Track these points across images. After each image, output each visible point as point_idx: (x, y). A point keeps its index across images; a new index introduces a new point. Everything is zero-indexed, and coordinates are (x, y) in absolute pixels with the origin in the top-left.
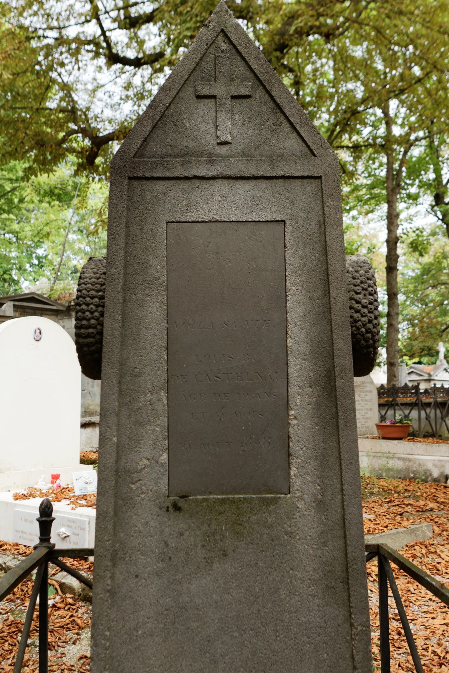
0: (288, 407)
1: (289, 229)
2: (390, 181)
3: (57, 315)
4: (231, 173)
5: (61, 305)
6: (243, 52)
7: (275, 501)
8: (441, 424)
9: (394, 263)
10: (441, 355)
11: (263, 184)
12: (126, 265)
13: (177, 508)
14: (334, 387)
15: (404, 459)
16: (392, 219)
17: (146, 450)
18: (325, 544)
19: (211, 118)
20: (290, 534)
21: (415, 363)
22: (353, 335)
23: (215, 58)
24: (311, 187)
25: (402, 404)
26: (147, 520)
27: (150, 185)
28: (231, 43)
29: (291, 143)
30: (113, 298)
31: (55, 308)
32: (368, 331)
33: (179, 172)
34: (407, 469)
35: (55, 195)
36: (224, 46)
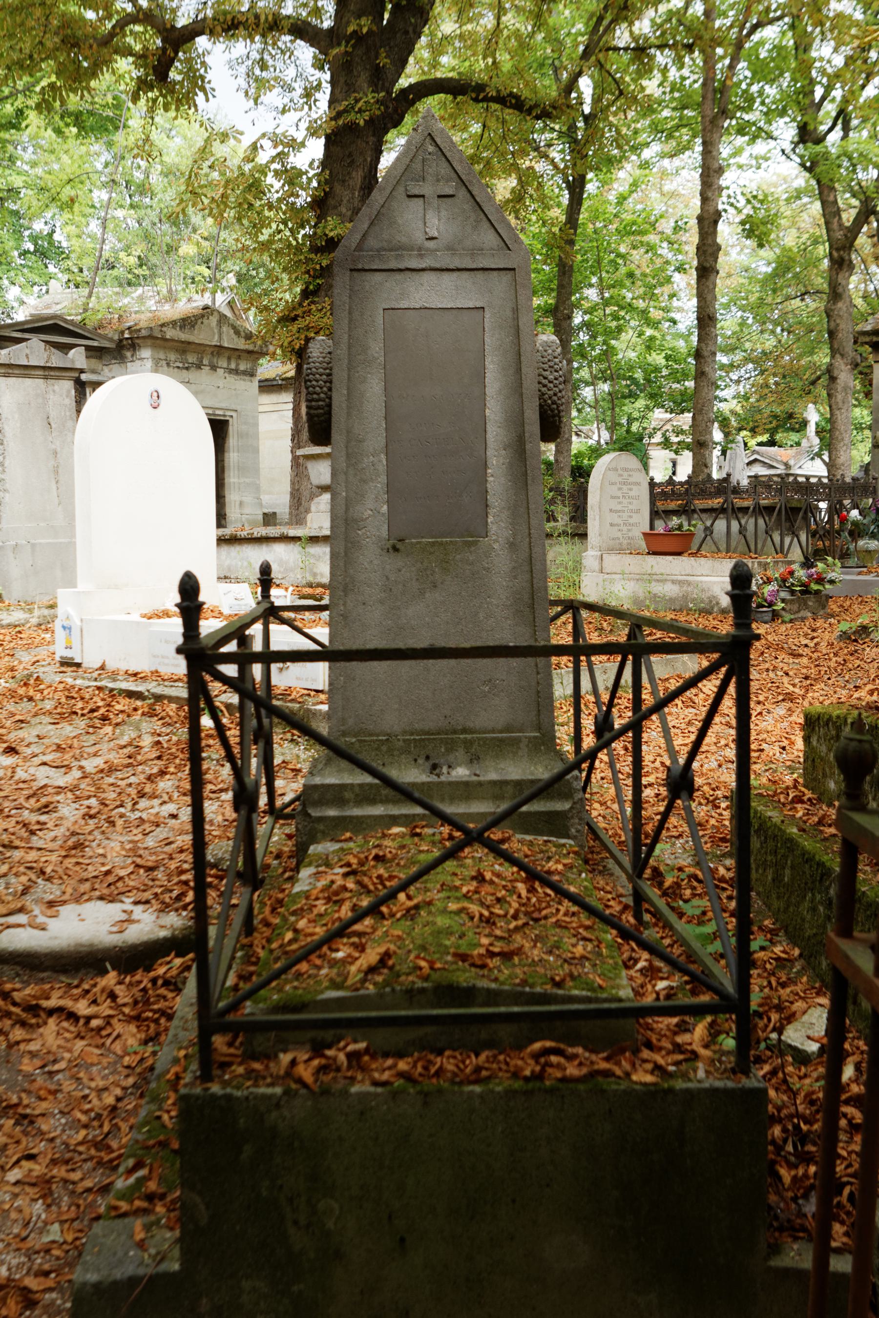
0: (486, 466)
1: (487, 315)
2: (709, 102)
3: (100, 358)
4: (438, 266)
5: (105, 337)
6: (448, 154)
7: (475, 543)
8: (765, 540)
9: (711, 259)
10: (811, 429)
11: (465, 275)
12: (350, 347)
13: (395, 549)
14: (524, 451)
15: (680, 583)
16: (710, 173)
17: (370, 503)
18: (515, 577)
19: (421, 215)
20: (487, 570)
21: (760, 444)
22: (541, 406)
23: (424, 160)
24: (506, 277)
25: (704, 511)
26: (371, 560)
27: (368, 276)
28: (437, 145)
29: (489, 238)
30: (340, 375)
31: (95, 344)
32: (554, 403)
33: (393, 265)
34: (685, 597)
35: (70, 115)
36: (431, 148)
